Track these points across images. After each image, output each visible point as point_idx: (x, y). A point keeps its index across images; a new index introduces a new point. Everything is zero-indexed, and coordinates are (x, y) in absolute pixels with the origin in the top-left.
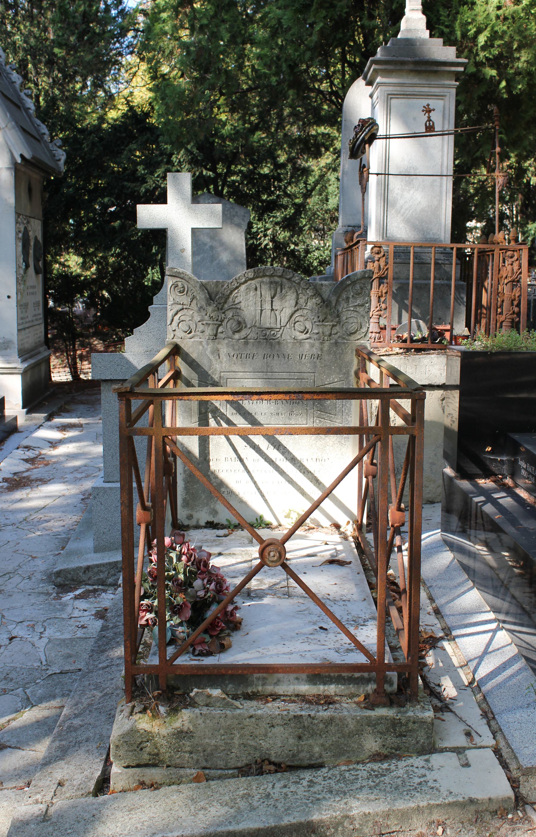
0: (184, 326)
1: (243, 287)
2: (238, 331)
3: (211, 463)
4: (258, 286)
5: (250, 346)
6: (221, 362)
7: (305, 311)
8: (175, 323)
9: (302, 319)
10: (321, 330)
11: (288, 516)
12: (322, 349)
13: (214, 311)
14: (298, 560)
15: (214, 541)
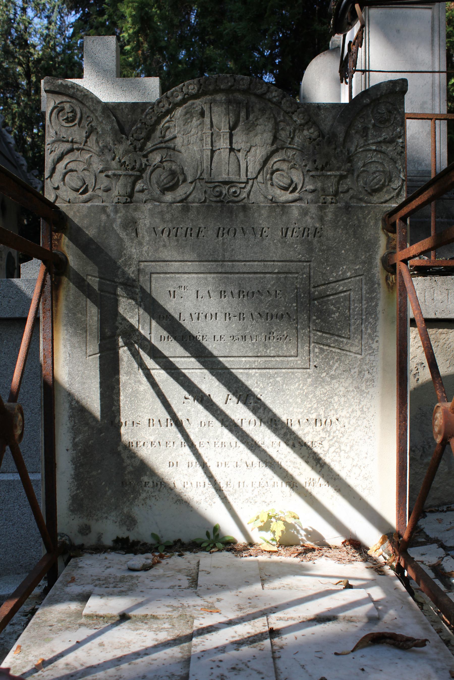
0: (73, 180)
1: (179, 112)
2: (172, 188)
3: (123, 430)
4: (206, 108)
5: (192, 214)
6: (140, 244)
7: (291, 153)
8: (57, 176)
9: (285, 166)
10: (319, 184)
11: (266, 527)
12: (321, 219)
13: (127, 152)
14: (299, 633)
15: (122, 579)
